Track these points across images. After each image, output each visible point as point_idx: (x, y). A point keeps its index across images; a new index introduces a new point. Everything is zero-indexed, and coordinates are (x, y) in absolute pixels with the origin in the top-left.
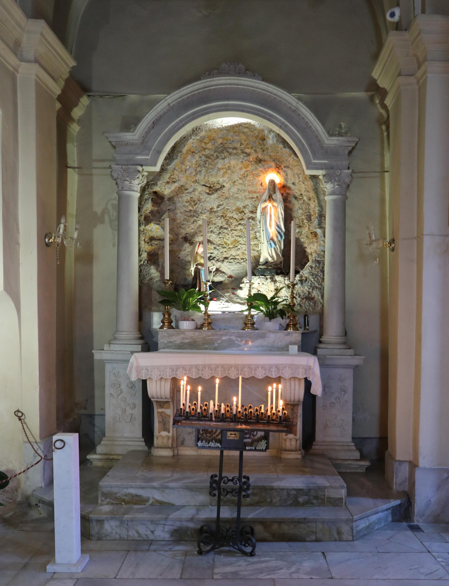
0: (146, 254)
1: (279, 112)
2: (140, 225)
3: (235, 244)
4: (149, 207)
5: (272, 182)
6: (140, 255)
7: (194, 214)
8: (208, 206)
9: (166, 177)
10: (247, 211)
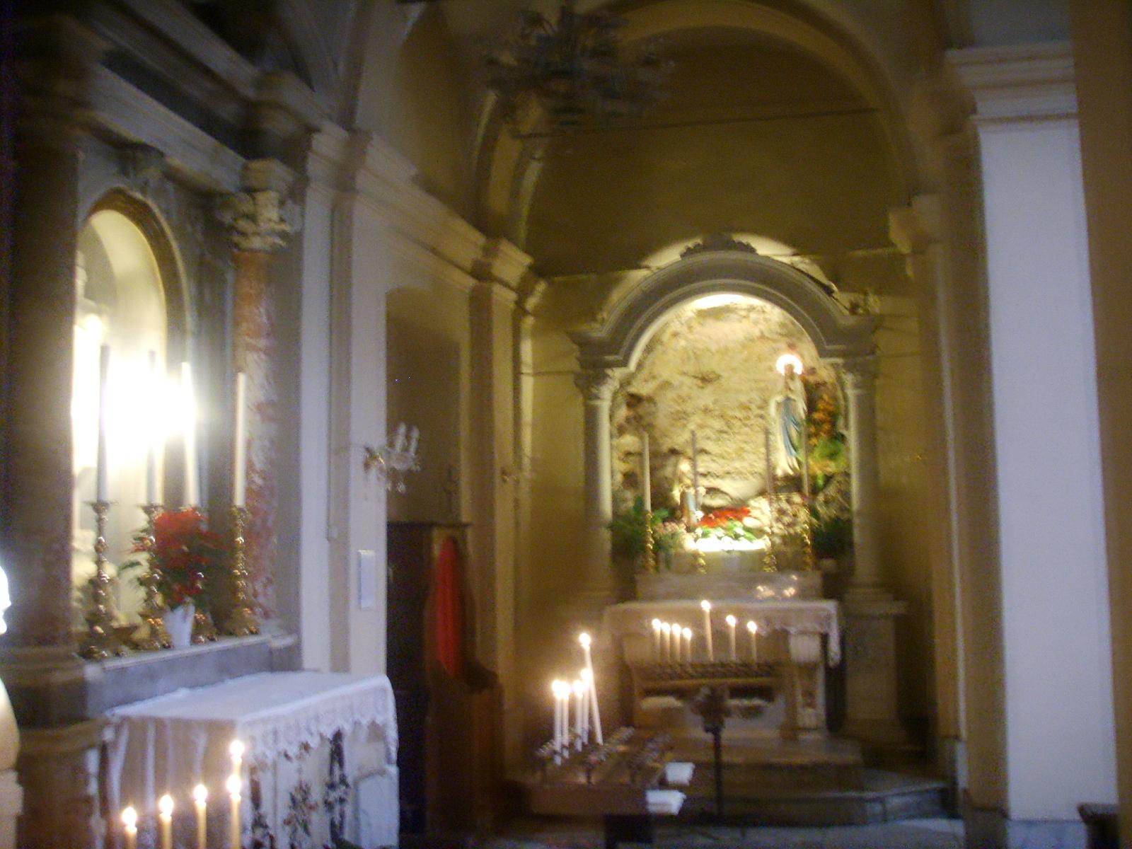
0: (626, 491)
1: (715, 276)
2: (612, 436)
3: (740, 453)
4: (623, 412)
5: (790, 368)
6: (612, 476)
7: (682, 417)
8: (701, 403)
9: (645, 373)
10: (753, 407)
